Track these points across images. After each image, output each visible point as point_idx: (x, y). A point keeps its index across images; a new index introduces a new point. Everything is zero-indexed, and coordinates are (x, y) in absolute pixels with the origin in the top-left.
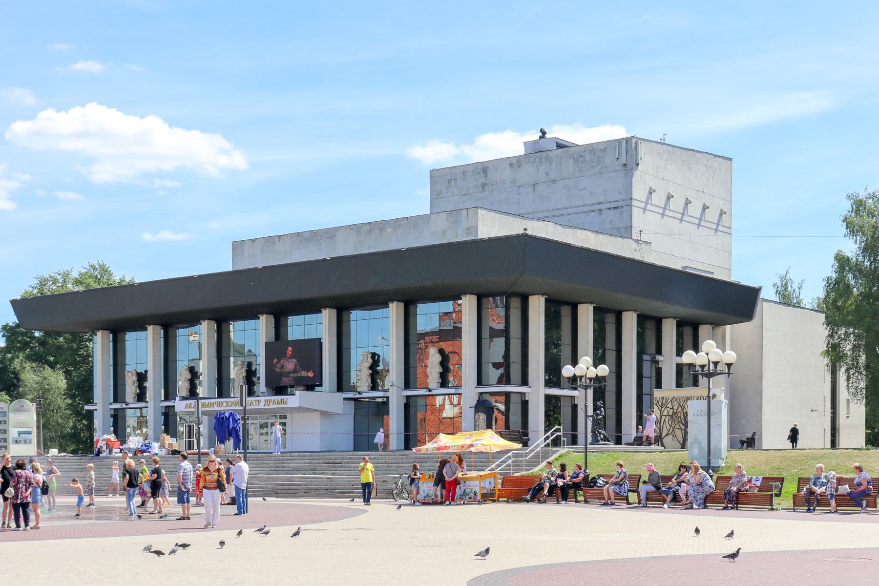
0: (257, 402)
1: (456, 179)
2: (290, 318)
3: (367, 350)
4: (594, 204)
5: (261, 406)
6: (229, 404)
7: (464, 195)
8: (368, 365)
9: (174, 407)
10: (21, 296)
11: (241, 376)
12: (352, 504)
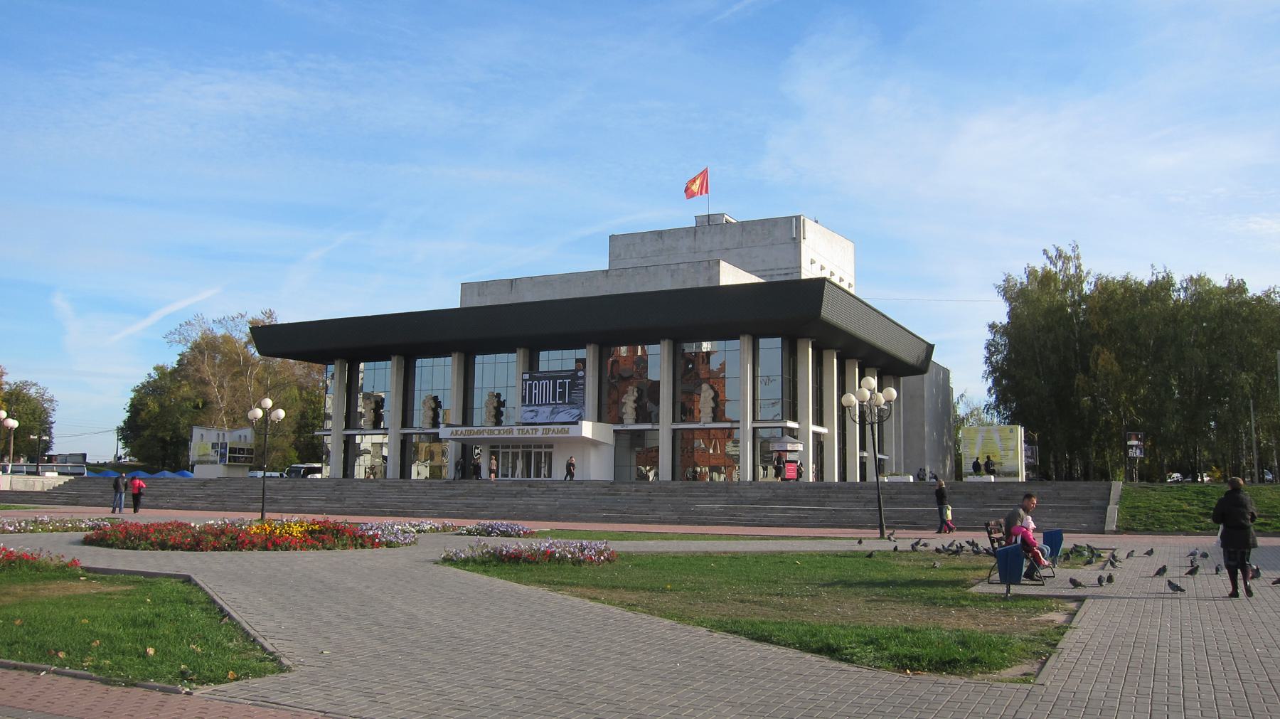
0: (534, 431)
1: (634, 244)
2: (760, 340)
3: (430, 392)
4: (765, 270)
5: (539, 434)
6: (502, 432)
7: (642, 258)
8: (634, 398)
9: (438, 434)
10: (253, 318)
11: (491, 407)
12: (919, 536)
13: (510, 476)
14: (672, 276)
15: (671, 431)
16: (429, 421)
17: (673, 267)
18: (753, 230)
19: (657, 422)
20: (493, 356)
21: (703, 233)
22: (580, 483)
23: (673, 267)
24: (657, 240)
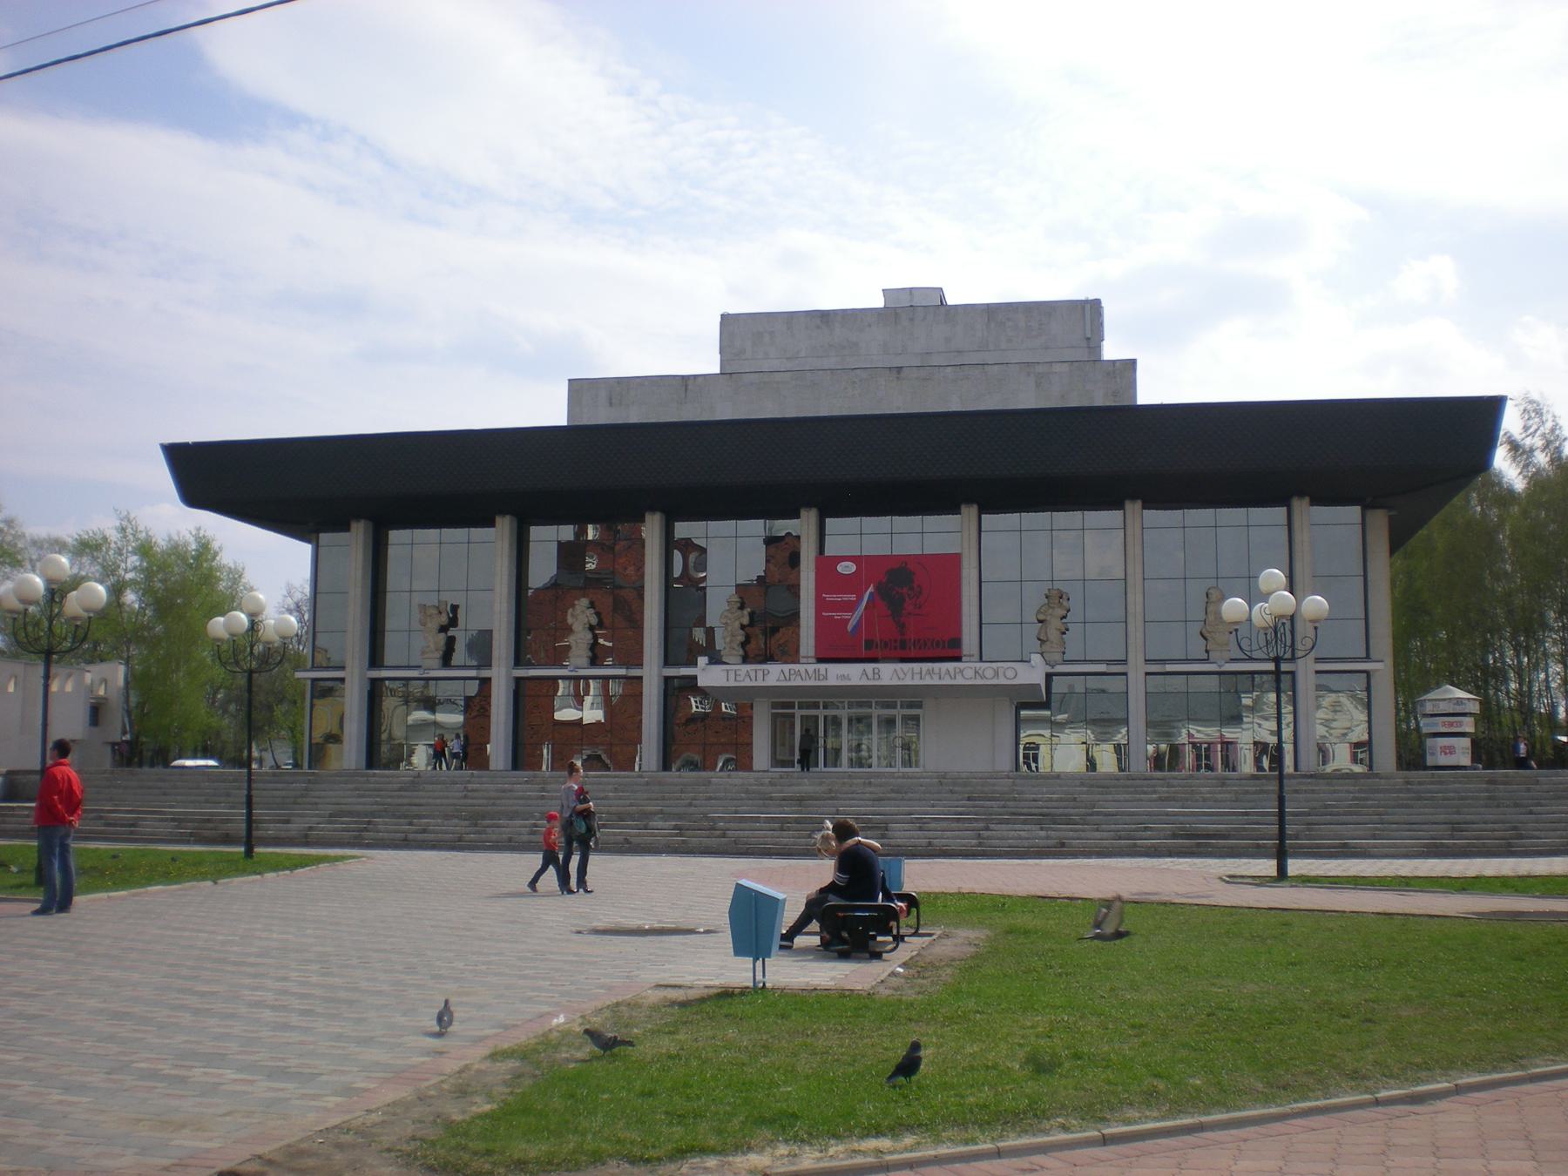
9: (695, 677)
13: (306, 764)
14: (1038, 385)
15: (663, 678)
16: (435, 657)
17: (1039, 369)
18: (1009, 319)
19: (640, 665)
20: (1210, 511)
21: (912, 320)
22: (1046, 777)
23: (1039, 369)
24: (818, 327)
